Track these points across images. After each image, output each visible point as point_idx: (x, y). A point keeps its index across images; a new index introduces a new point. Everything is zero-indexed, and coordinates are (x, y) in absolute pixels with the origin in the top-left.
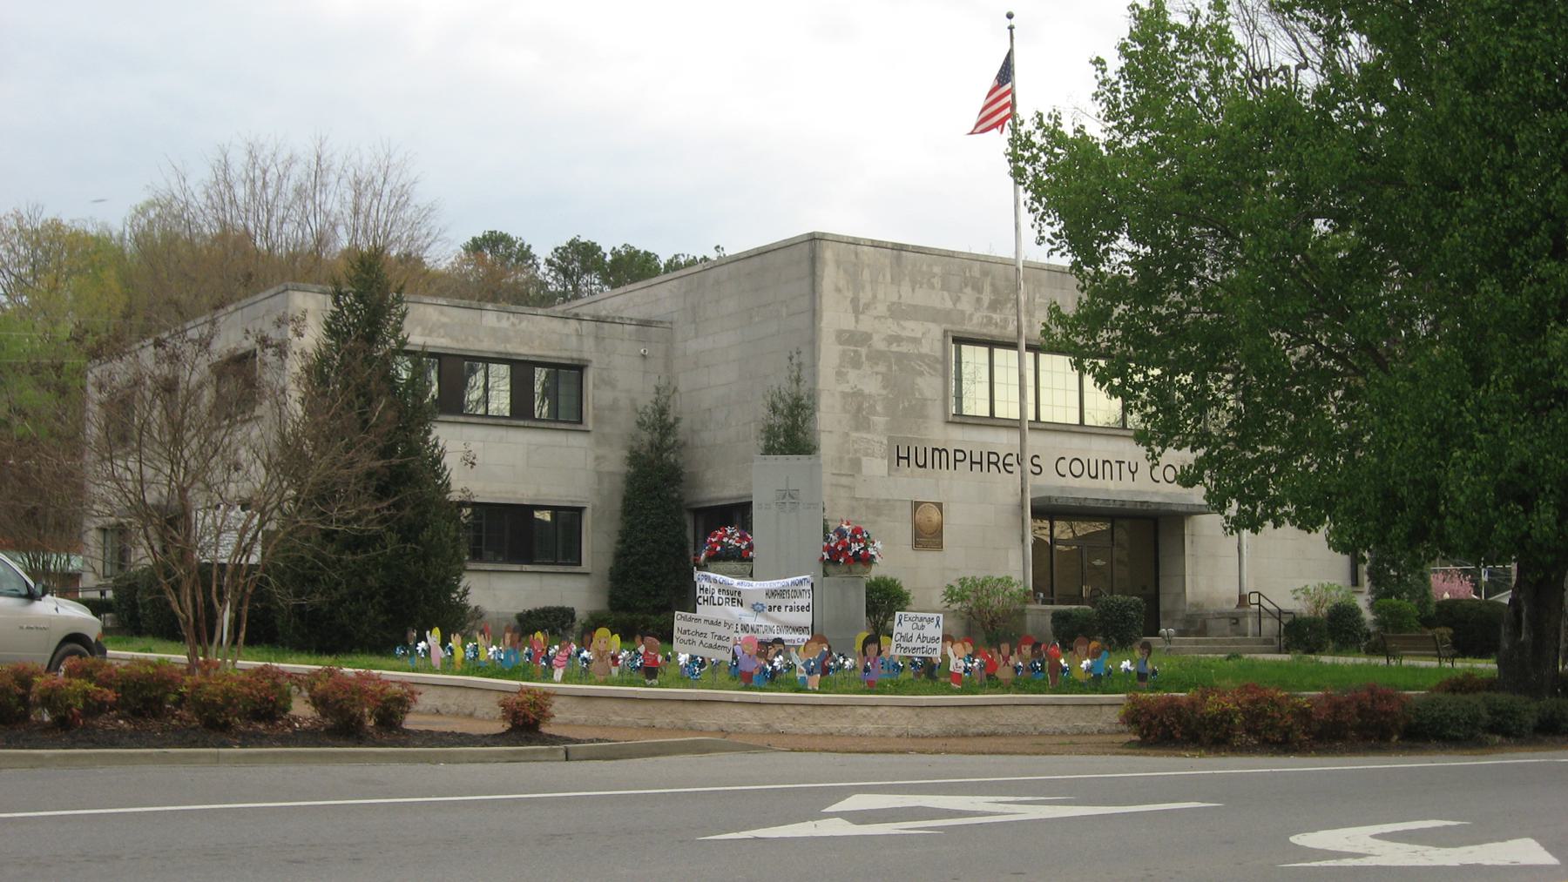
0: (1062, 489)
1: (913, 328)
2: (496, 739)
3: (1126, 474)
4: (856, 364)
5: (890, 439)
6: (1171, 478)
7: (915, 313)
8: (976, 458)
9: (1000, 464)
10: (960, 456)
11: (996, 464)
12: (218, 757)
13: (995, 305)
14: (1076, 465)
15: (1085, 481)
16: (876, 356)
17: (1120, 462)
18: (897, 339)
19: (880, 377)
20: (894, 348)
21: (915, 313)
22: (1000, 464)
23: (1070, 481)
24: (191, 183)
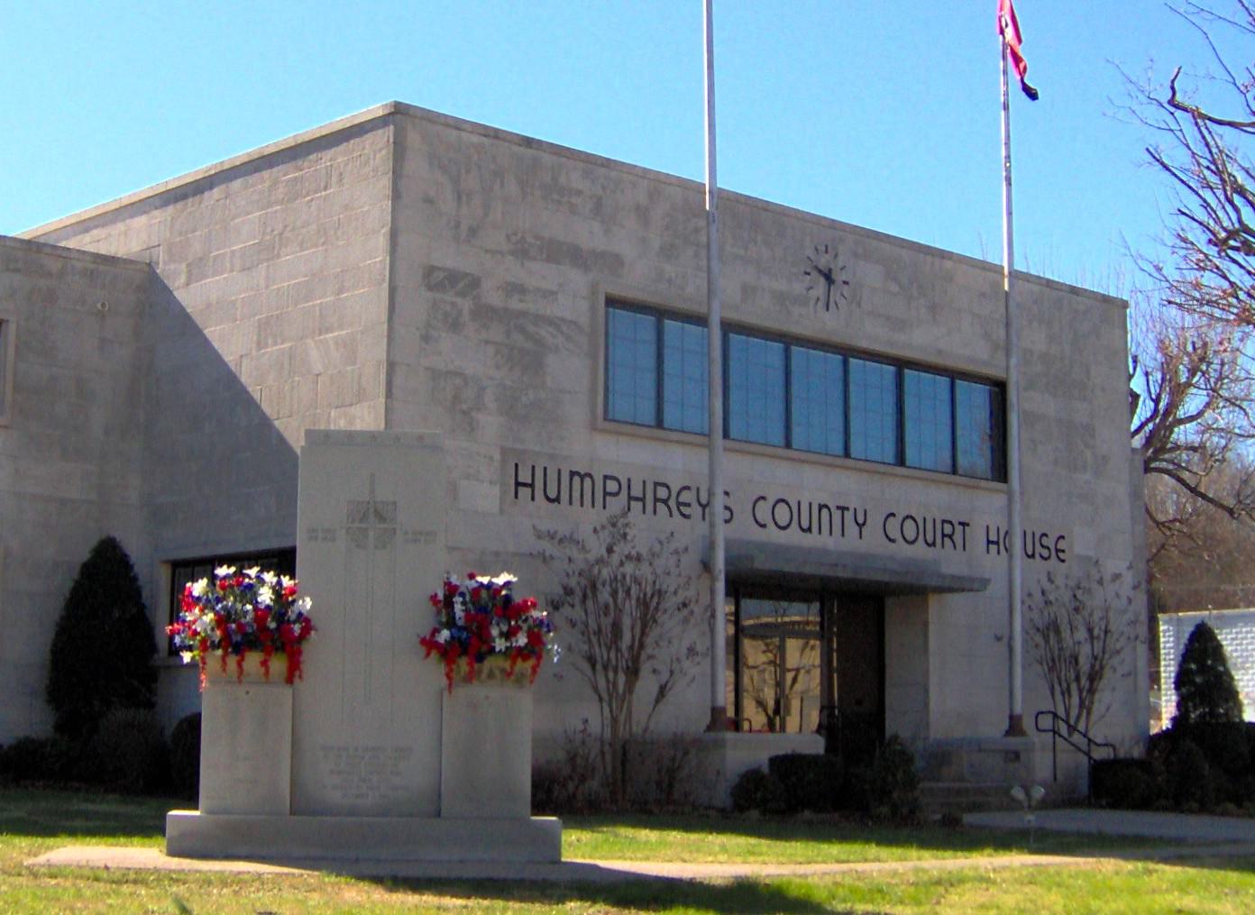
0: (762, 547)
1: (539, 274)
2: (1011, 710)
3: (852, 529)
4: (455, 326)
5: (504, 451)
6: (910, 535)
7: (556, 252)
8: (637, 491)
9: (672, 503)
10: (612, 486)
11: (665, 502)
12: (230, 813)
13: (668, 252)
14: (909, 524)
15: (793, 537)
16: (484, 313)
17: (843, 509)
18: (518, 289)
19: (491, 350)
20: (515, 304)
21: (556, 252)
22: (672, 503)
23: (773, 535)
24: (716, 305)
